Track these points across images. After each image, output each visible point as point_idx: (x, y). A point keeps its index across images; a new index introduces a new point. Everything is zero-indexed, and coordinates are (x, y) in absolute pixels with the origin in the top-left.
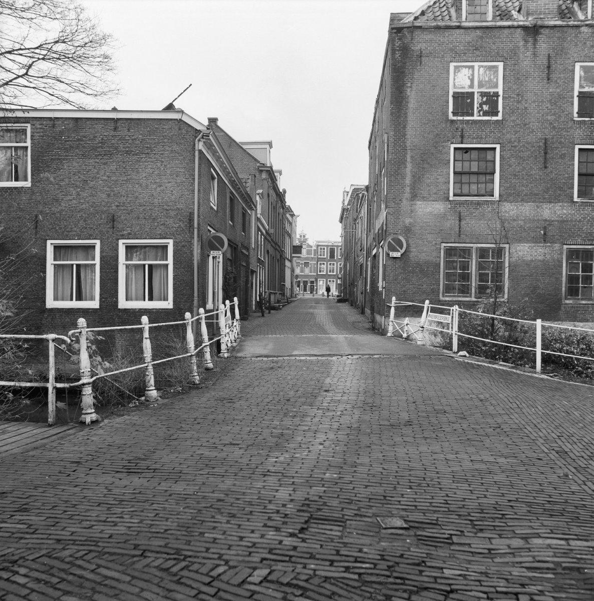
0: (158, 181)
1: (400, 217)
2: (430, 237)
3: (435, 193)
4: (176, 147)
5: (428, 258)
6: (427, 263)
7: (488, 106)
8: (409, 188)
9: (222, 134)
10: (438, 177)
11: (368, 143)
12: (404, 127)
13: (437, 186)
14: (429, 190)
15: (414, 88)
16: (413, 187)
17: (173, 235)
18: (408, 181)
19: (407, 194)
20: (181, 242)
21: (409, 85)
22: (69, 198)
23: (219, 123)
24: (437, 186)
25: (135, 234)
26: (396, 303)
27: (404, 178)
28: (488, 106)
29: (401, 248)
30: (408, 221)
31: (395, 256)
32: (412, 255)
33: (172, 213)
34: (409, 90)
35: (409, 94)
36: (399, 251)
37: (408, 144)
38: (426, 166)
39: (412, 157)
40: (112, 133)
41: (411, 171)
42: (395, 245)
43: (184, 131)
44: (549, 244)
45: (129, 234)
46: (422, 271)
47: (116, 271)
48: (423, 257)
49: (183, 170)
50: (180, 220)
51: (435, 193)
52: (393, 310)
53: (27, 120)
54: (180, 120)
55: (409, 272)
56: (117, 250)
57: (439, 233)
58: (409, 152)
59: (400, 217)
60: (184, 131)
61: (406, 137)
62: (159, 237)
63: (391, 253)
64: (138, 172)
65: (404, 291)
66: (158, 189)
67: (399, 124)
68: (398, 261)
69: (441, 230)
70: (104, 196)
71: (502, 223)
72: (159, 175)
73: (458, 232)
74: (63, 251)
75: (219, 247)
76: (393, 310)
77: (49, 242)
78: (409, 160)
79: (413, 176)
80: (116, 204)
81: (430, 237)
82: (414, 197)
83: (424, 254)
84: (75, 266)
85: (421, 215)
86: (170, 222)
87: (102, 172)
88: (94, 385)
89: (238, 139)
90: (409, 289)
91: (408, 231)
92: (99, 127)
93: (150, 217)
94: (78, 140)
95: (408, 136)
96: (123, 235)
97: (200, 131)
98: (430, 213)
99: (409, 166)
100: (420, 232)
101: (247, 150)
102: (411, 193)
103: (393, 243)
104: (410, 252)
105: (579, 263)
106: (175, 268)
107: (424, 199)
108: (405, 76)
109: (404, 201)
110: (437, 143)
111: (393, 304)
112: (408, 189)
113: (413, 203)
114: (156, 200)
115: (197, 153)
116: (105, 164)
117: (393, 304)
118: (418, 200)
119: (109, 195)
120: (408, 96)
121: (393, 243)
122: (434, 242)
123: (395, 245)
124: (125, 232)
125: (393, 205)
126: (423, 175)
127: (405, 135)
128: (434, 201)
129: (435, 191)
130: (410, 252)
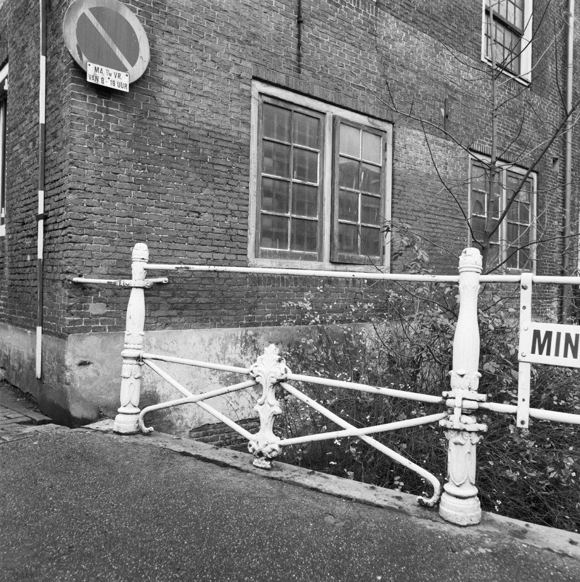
5: (216, 120)
7: (335, 443)
11: (291, 101)
26: (150, 274)
28: (335, 443)
31: (108, 84)
32: (166, 96)
44: (451, 143)
46: (198, 160)
52: (137, 304)
68: (116, 108)
69: (254, 36)
71: (385, 61)
73: (294, 58)
76: (137, 304)
88: (309, 203)
105: (358, 194)
111: (138, 277)
117: (138, 277)
122: (233, 70)
123: (110, 41)
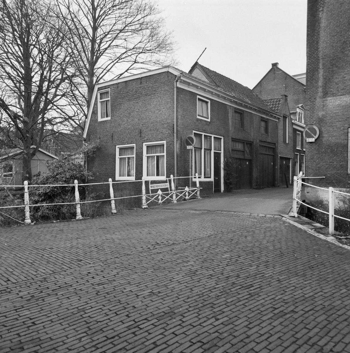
0: (159, 108)
1: (315, 111)
2: (338, 124)
3: (342, 89)
4: (166, 88)
6: (337, 145)
8: (321, 88)
9: (281, 72)
10: (345, 76)
12: (317, 43)
13: (345, 83)
14: (338, 87)
15: (325, 10)
16: (325, 87)
17: (166, 138)
18: (320, 83)
19: (320, 94)
20: (169, 142)
21: (321, 9)
22: (124, 123)
23: (280, 66)
24: (345, 83)
25: (150, 139)
27: (317, 82)
29: (315, 135)
30: (321, 114)
31: (310, 141)
33: (165, 126)
34: (321, 13)
35: (321, 16)
36: (313, 137)
37: (321, 55)
38: (335, 69)
39: (323, 64)
40: (140, 86)
41: (323, 75)
42: (311, 133)
43: (170, 78)
45: (147, 139)
46: (332, 151)
47: (142, 160)
48: (333, 140)
49: (170, 100)
50: (169, 129)
51: (342, 89)
53: (108, 87)
54: (168, 71)
55: (322, 153)
56: (142, 148)
57: (347, 120)
58: (321, 61)
59: (315, 111)
60: (170, 78)
61: (319, 50)
62: (159, 140)
63: (307, 139)
64: (150, 105)
65: (319, 167)
66: (159, 113)
67: (314, 41)
68: (314, 145)
70: (137, 120)
72: (160, 105)
74: (123, 151)
75: (313, 135)
77: (117, 146)
78: (321, 67)
79: (325, 79)
80: (142, 123)
81: (338, 124)
82: (326, 94)
83: (334, 138)
84: (156, 157)
85: (331, 108)
86: (164, 130)
87: (136, 108)
89: (291, 74)
90: (323, 166)
91: (321, 121)
92: (134, 84)
93: (156, 129)
94: (127, 92)
95: (320, 49)
96: (144, 140)
97: (176, 76)
98: (339, 105)
99: (321, 72)
100: (330, 121)
101: (298, 80)
102: (323, 92)
103: (309, 132)
104: (323, 137)
106: (167, 157)
107: (333, 95)
108: (317, 4)
109: (318, 99)
110: (344, 48)
112: (320, 90)
113: (324, 99)
114: (158, 119)
115: (175, 89)
116: (137, 103)
118: (329, 97)
119: (139, 119)
120: (320, 18)
121: (309, 132)
122: (342, 128)
123: (311, 133)
124: (146, 139)
125: (309, 103)
126: (332, 76)
127: (318, 48)
128: (341, 95)
129: (342, 87)
130: (323, 137)
